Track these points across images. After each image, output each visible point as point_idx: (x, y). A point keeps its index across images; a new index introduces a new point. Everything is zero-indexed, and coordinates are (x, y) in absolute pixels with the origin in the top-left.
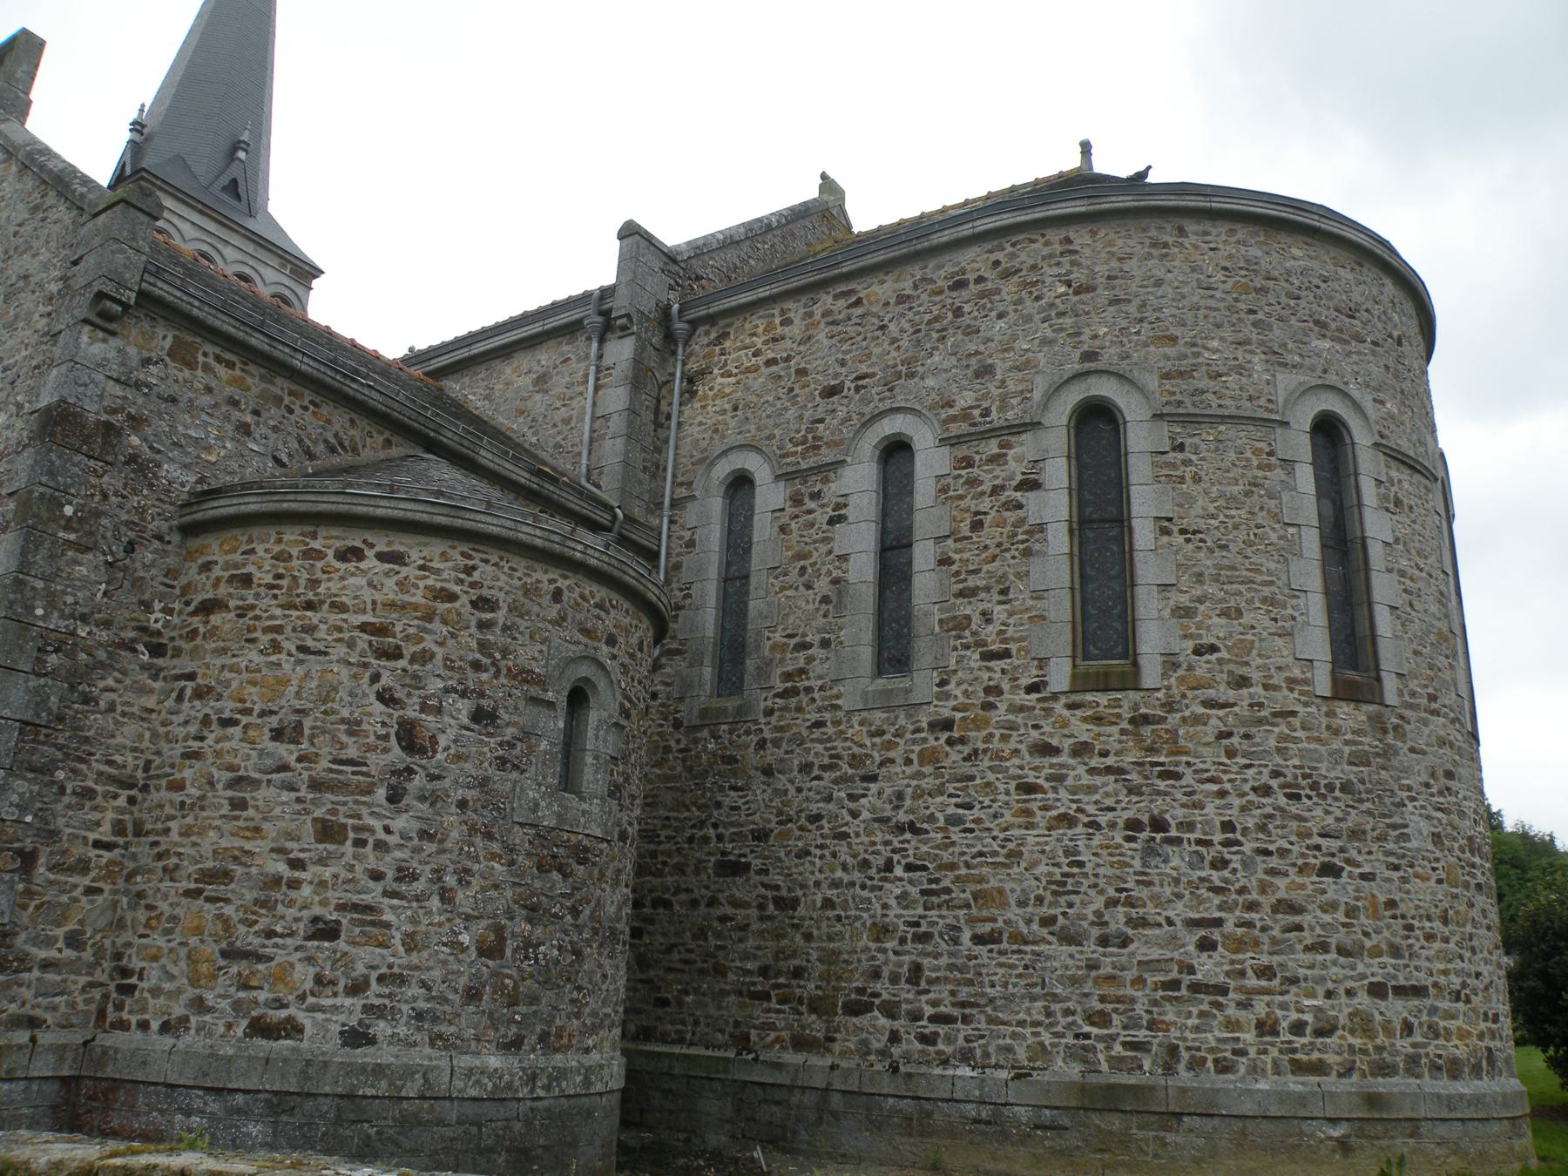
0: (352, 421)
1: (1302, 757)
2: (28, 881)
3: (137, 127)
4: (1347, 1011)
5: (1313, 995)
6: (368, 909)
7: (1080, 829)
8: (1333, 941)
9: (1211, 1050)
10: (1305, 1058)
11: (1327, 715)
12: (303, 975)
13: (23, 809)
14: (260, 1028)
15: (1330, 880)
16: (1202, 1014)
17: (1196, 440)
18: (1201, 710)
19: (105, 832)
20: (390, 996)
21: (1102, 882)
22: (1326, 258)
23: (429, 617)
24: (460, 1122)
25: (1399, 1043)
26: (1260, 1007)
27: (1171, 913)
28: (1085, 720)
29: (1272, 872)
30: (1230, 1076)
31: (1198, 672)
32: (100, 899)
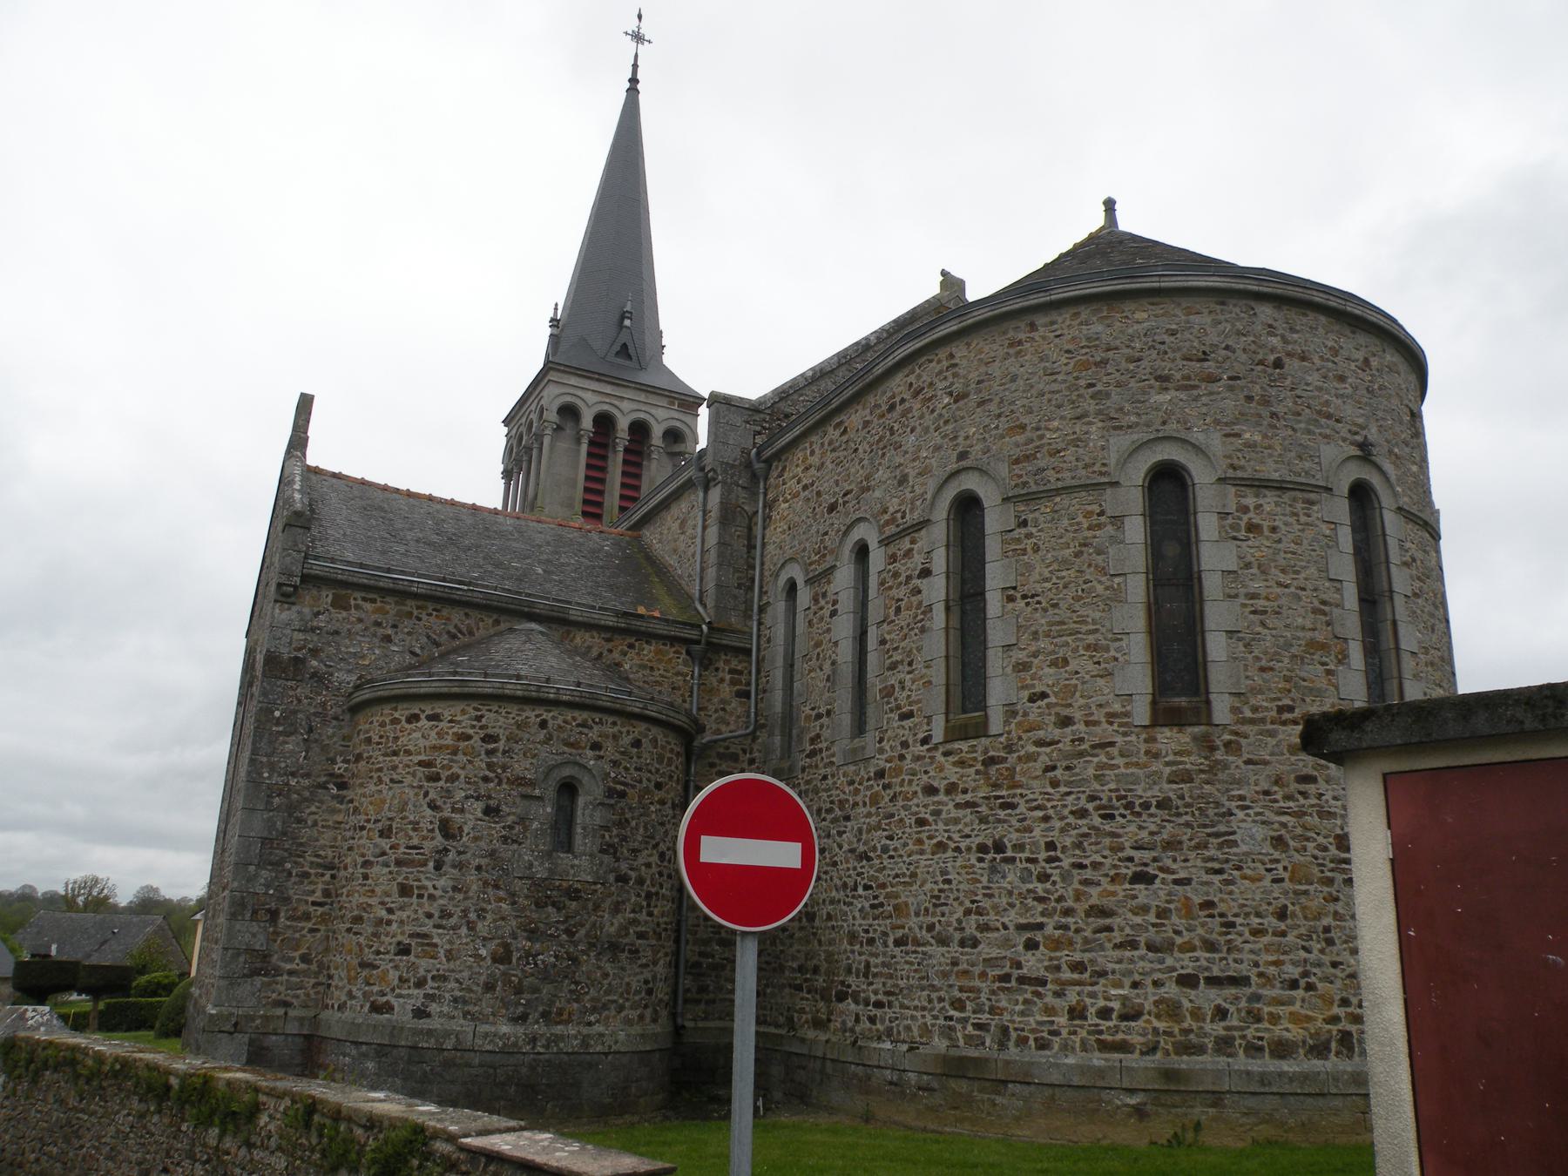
0: (466, 615)
1: (1118, 781)
2: (276, 926)
3: (554, 322)
4: (1152, 999)
5: (1119, 985)
6: (425, 936)
7: (950, 853)
8: (1142, 940)
9: (1033, 1031)
10: (1110, 1038)
11: (1146, 741)
12: (393, 976)
13: (268, 886)
14: (376, 1008)
15: (1142, 887)
16: (1026, 1002)
17: (1037, 514)
18: (1034, 749)
19: (318, 896)
20: (438, 988)
21: (961, 895)
22: (1178, 312)
23: (455, 753)
24: (481, 1065)
25: (1208, 1027)
26: (1072, 996)
27: (1005, 920)
28: (954, 764)
29: (1086, 882)
30: (1047, 1053)
31: (1031, 717)
32: (319, 935)
